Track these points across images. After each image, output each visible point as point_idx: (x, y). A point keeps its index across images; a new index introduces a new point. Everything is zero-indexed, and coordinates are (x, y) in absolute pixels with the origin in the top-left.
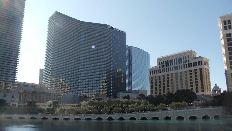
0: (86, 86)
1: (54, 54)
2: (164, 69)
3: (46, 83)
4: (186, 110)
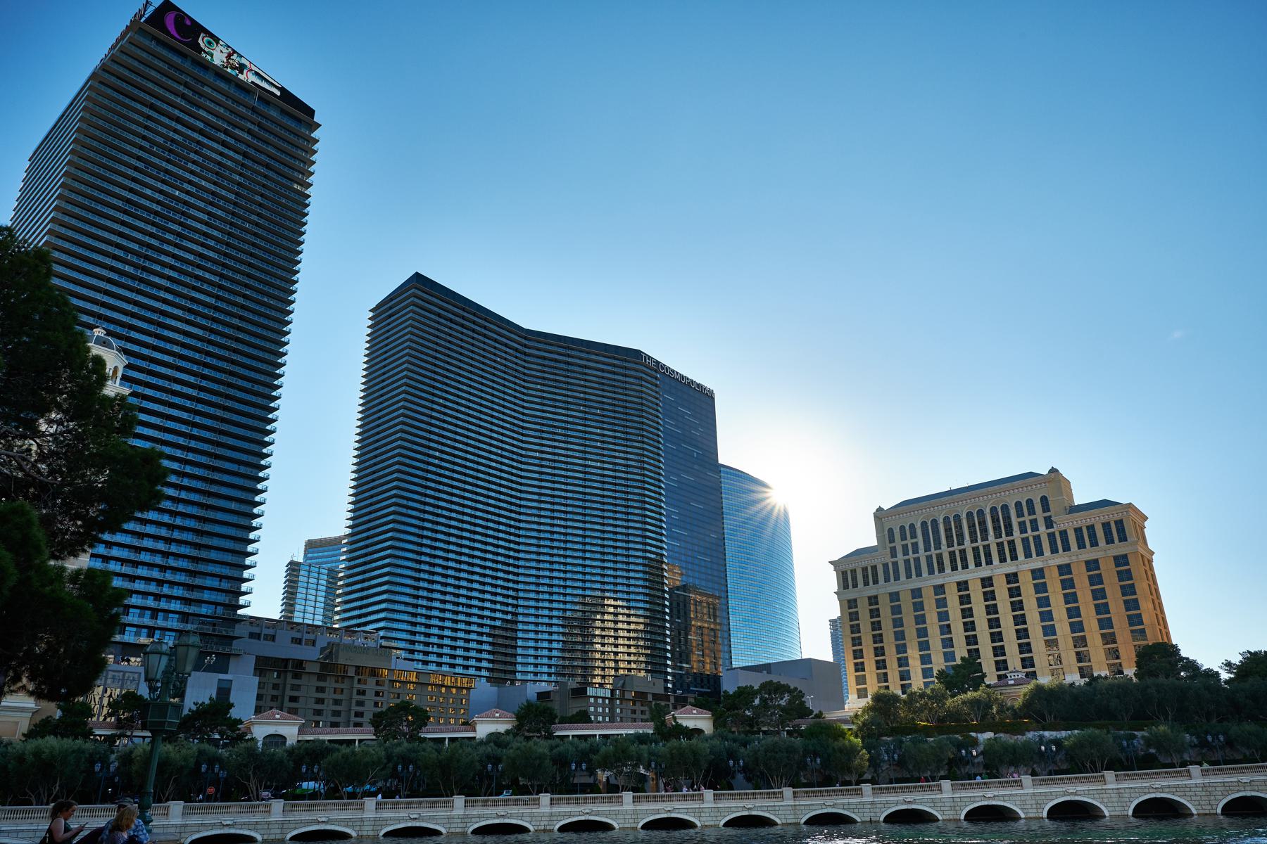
4: (1112, 785)
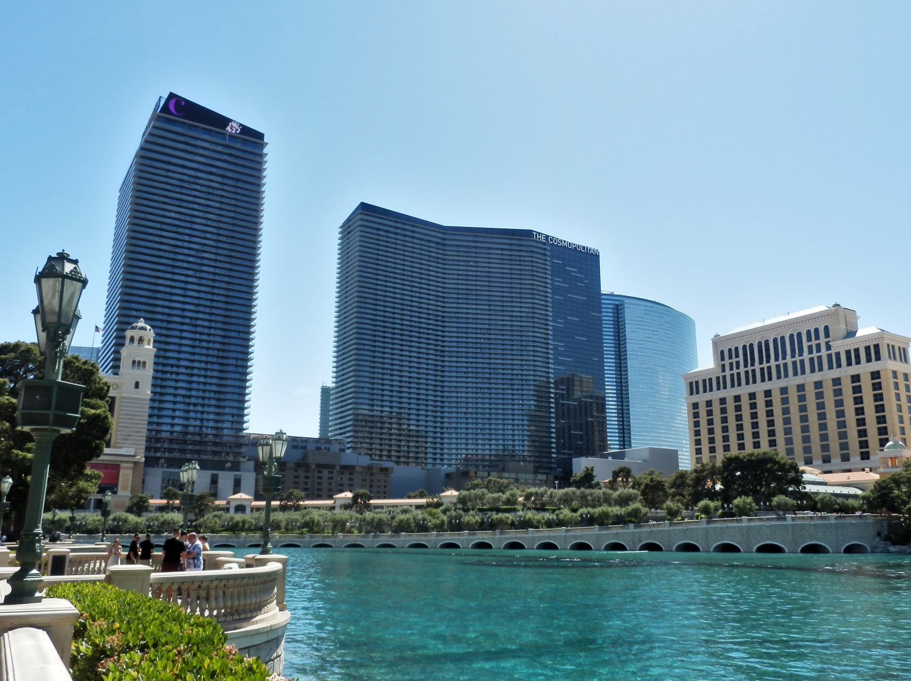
0: (467, 439)
2: (739, 374)
3: (341, 434)
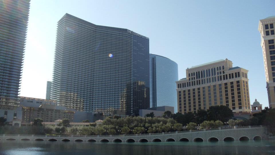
0: (101, 102)
1: (63, 63)
2: (195, 81)
3: (55, 98)
